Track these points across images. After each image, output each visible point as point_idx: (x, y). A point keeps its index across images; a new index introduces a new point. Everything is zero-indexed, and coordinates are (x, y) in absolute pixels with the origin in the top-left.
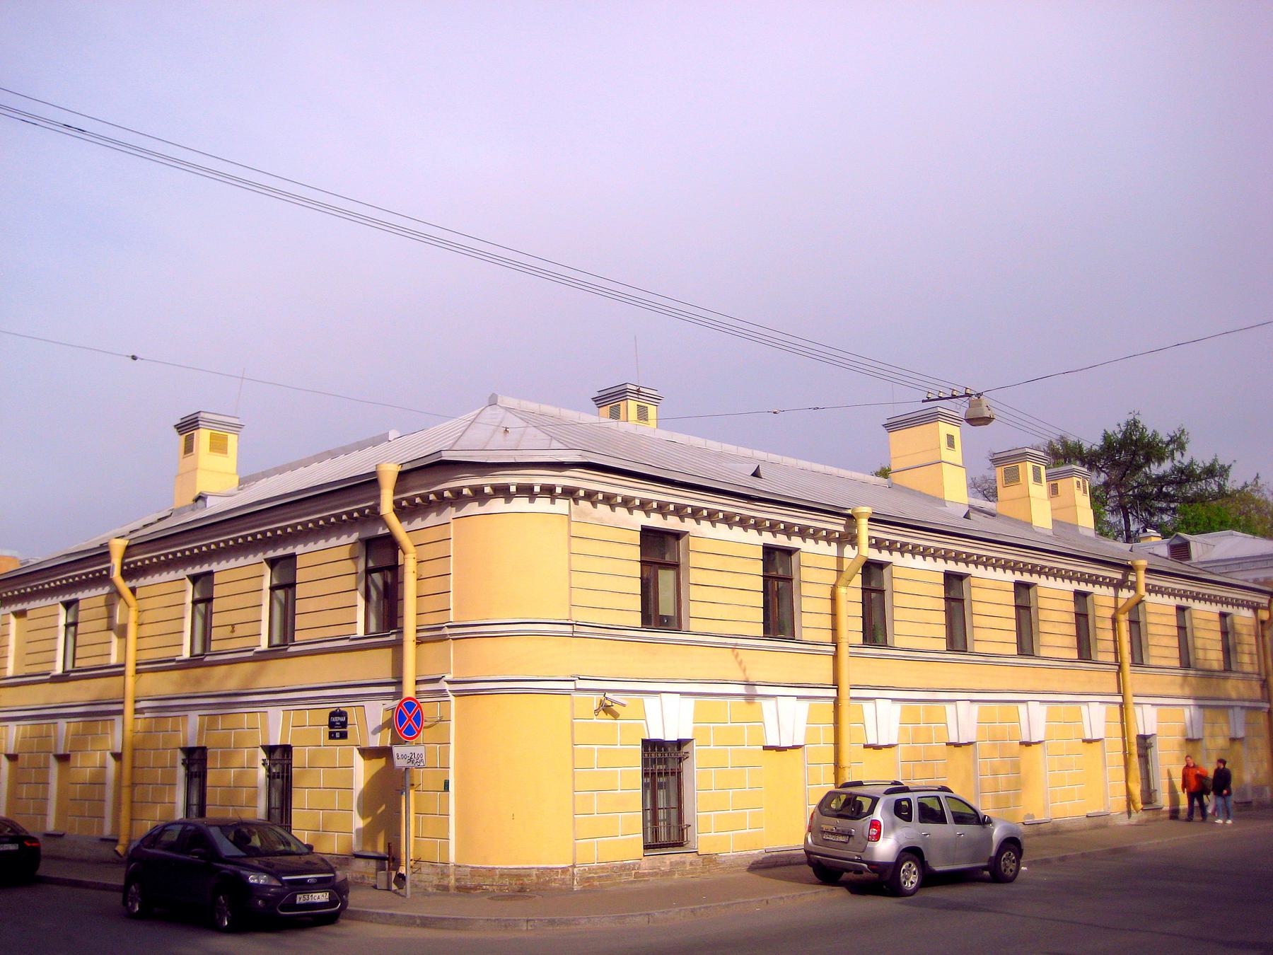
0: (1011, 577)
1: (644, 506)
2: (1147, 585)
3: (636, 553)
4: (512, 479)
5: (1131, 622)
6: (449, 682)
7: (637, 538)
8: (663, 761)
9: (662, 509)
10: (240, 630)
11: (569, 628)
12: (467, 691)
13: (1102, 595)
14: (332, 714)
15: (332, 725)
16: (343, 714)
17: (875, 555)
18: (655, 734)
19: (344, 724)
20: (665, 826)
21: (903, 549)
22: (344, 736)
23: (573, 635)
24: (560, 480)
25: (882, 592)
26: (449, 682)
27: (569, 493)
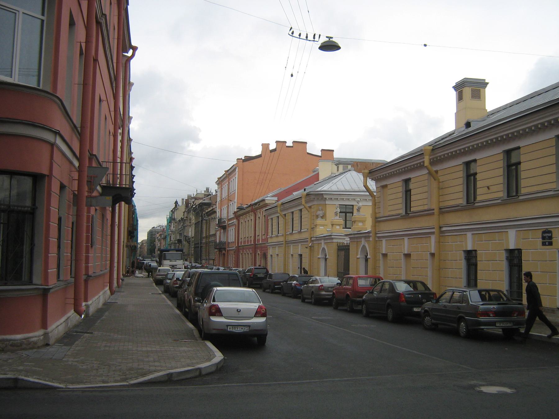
10: (493, 189)
14: (544, 232)
15: (543, 238)
16: (550, 232)
19: (551, 238)
22: (551, 244)
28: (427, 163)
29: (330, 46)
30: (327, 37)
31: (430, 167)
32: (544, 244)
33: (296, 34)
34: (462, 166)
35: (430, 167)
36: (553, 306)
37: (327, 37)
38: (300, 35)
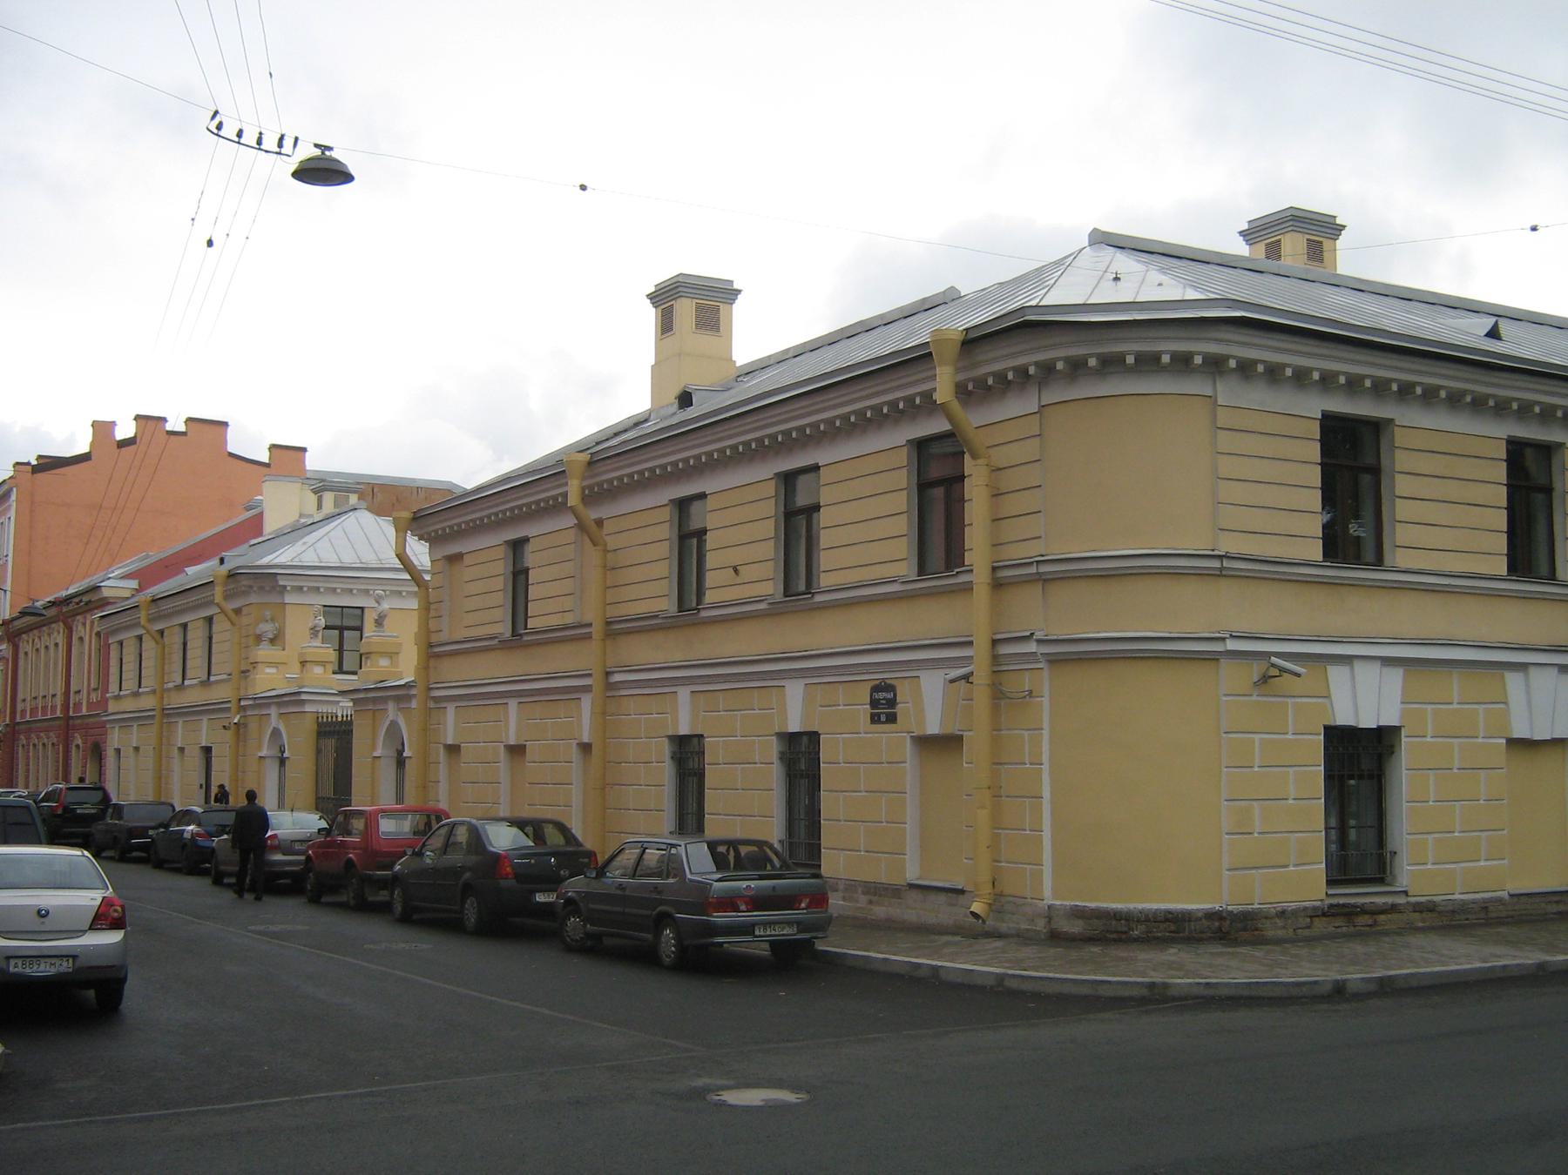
0: (1315, 405)
1: (1327, 381)
4: (1130, 348)
6: (1039, 641)
9: (1353, 385)
10: (747, 573)
11: (1216, 564)
12: (1072, 657)
14: (876, 689)
15: (874, 703)
18: (1343, 718)
19: (892, 703)
21: (1429, 397)
22: (892, 719)
23: (1221, 574)
24: (1200, 347)
26: (1039, 641)
27: (1215, 365)
29: (322, 171)
30: (317, 146)
31: (956, 407)
32: (875, 719)
33: (229, 131)
37: (317, 146)
38: (240, 134)
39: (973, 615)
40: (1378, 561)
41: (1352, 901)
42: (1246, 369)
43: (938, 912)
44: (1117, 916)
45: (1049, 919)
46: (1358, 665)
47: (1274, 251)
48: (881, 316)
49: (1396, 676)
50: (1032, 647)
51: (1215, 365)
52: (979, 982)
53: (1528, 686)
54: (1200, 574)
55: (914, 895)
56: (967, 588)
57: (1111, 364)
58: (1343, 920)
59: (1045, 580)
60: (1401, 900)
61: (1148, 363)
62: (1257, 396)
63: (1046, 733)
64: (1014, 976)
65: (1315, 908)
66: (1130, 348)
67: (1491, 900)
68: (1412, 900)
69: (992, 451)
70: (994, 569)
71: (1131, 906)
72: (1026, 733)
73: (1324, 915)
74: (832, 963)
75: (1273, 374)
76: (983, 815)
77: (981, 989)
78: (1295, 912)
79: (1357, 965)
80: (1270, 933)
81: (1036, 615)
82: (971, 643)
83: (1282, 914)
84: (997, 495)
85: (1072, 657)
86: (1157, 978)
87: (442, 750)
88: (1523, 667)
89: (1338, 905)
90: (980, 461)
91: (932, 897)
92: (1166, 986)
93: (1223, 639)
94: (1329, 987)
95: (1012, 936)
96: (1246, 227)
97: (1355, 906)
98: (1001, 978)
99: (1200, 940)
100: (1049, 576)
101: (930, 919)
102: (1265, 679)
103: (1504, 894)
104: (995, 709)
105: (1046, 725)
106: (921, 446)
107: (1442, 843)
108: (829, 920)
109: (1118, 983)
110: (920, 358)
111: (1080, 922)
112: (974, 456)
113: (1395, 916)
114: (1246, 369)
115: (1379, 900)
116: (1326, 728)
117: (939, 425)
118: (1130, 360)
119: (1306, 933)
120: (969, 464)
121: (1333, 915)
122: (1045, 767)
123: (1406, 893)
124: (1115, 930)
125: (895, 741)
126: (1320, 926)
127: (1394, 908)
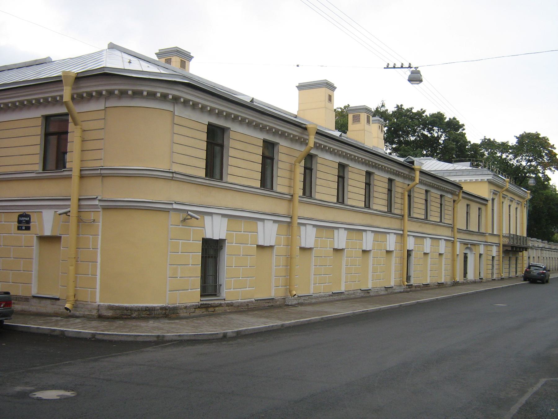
0: (206, 119)
1: (211, 112)
2: (315, 143)
3: (260, 151)
4: (146, 89)
5: (305, 168)
6: (99, 200)
7: (261, 144)
8: (212, 249)
9: (219, 114)
11: (171, 175)
12: (111, 207)
13: (398, 181)
15: (19, 222)
16: (29, 216)
17: (313, 152)
18: (209, 236)
19: (28, 222)
20: (210, 282)
21: (242, 121)
22: (28, 228)
23: (172, 179)
24: (172, 92)
25: (222, 146)
26: (99, 200)
27: (176, 100)
28: (67, 98)
31: (71, 104)
32: (19, 228)
34: (41, 119)
35: (71, 104)
36: (27, 294)
39: (72, 188)
40: (221, 178)
41: (208, 302)
42: (186, 102)
43: (48, 307)
44: (127, 309)
45: (98, 310)
46: (214, 216)
47: (168, 61)
48: (36, 61)
49: (226, 220)
50: (97, 202)
51: (176, 100)
52: (85, 336)
53: (264, 227)
54: (165, 178)
55: (35, 300)
56: (69, 177)
57: (137, 94)
58: (206, 310)
59: (103, 176)
60: (223, 302)
61: (152, 96)
62: (187, 113)
63: (100, 237)
64: (100, 334)
65: (196, 305)
66: (146, 89)
67: (249, 302)
68: (226, 302)
69: (84, 123)
70: (81, 170)
71: (132, 305)
72: (91, 236)
73: (199, 308)
74: (12, 330)
75: (195, 106)
76: (72, 268)
77: (86, 339)
78: (190, 307)
79: (208, 328)
80: (182, 315)
81: (97, 190)
82: (70, 199)
83: (186, 307)
84: (83, 141)
85: (111, 207)
86: (159, 333)
87: (35, 239)
88: (263, 220)
89: (203, 304)
90: (78, 127)
91: (44, 301)
92: (164, 336)
93: (172, 204)
94: (222, 335)
95: (82, 317)
96: (158, 52)
97: (209, 304)
98: (94, 335)
99: (158, 318)
100: (105, 175)
101: (43, 310)
102: (185, 220)
103: (253, 300)
104: (78, 226)
105: (100, 234)
106: (47, 118)
107: (239, 282)
108: (12, 312)
109: (144, 336)
110: (57, 82)
111: (111, 311)
112: (76, 124)
113: (220, 308)
114: (186, 102)
115: (216, 302)
116: (203, 239)
117: (64, 110)
118: (145, 93)
119: (193, 314)
120: (71, 127)
121: (202, 308)
122: (99, 250)
123: (224, 299)
124: (124, 314)
125: (29, 238)
126: (198, 312)
127: (220, 305)
